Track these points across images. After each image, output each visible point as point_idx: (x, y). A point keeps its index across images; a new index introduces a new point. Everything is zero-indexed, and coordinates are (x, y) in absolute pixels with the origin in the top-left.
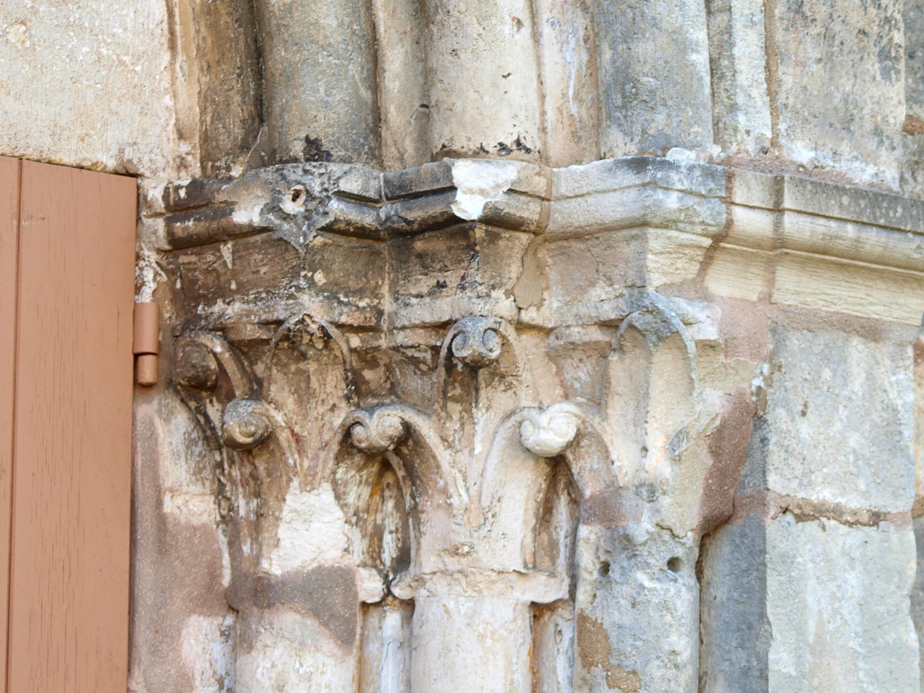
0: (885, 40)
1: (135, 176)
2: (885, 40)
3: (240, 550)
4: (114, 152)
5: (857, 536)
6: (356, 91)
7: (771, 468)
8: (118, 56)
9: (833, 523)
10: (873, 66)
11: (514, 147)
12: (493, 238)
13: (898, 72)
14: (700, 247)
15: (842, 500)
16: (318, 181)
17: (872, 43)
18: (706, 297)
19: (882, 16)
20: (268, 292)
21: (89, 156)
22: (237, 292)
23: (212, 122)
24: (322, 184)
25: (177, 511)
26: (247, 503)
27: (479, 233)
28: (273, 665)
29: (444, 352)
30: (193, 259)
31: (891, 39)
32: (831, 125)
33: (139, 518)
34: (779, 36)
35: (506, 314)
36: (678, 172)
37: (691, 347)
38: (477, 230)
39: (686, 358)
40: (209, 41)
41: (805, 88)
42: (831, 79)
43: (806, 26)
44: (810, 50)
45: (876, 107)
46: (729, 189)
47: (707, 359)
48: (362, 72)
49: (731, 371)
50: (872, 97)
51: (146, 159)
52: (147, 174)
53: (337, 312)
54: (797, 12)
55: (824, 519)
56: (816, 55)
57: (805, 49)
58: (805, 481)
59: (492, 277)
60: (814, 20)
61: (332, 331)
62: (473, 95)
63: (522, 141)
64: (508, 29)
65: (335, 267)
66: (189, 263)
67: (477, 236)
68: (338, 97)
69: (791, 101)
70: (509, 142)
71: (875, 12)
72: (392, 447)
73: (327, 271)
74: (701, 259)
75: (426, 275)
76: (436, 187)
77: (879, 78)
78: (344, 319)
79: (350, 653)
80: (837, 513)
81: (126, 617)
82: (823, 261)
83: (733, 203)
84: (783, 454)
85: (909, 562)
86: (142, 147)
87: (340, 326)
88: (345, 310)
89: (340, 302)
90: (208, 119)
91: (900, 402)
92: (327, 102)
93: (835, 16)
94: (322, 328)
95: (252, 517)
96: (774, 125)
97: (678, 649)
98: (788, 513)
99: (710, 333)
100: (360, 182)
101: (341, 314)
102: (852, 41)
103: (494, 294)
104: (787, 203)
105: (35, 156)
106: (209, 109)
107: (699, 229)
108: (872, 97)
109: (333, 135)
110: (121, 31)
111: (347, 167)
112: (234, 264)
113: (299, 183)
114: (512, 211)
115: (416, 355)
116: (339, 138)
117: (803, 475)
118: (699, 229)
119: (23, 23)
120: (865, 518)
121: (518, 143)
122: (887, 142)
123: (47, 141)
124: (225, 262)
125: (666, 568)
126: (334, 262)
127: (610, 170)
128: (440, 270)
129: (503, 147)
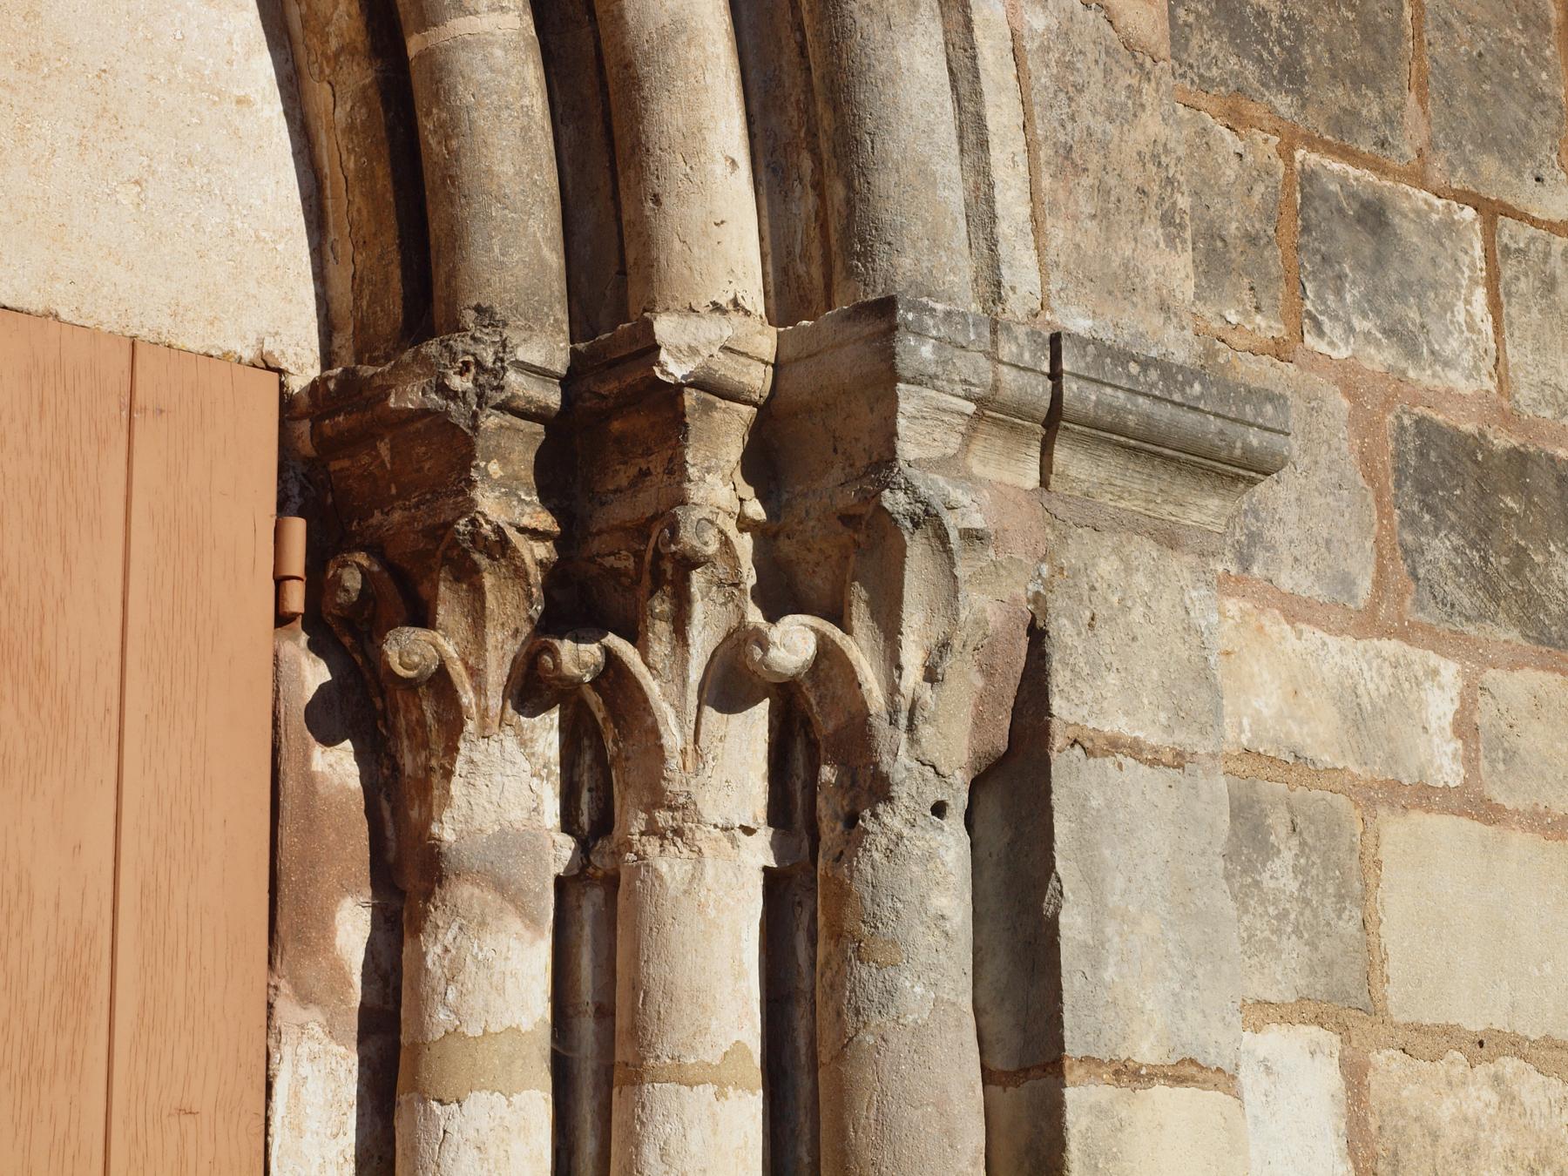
0: (1167, 205)
1: (280, 372)
2: (1167, 205)
3: (407, 816)
4: (252, 341)
5: (1160, 776)
6: (539, 250)
7: (1055, 689)
8: (256, 231)
9: (1131, 761)
10: (1153, 231)
11: (731, 307)
12: (708, 408)
13: (1184, 241)
14: (962, 414)
15: (1141, 735)
16: (491, 351)
17: (1152, 205)
18: (969, 480)
19: (1163, 175)
20: (433, 493)
21: (217, 345)
22: (398, 496)
23: (369, 306)
24: (496, 353)
25: (327, 770)
26: (414, 759)
27: (690, 398)
28: (446, 950)
29: (648, 557)
30: (346, 463)
31: (1174, 203)
32: (1110, 293)
33: (282, 776)
34: (1046, 182)
35: (724, 504)
36: (933, 317)
37: (954, 535)
38: (686, 397)
39: (948, 552)
40: (365, 213)
41: (1078, 246)
42: (1108, 240)
43: (1076, 175)
44: (1082, 203)
45: (1161, 279)
46: (994, 343)
47: (973, 554)
48: (545, 230)
49: (1002, 572)
50: (1156, 267)
51: (290, 352)
52: (292, 369)
53: (517, 511)
54: (1066, 158)
55: (1120, 757)
56: (1088, 209)
57: (1077, 203)
58: (1096, 708)
59: (707, 458)
60: (1085, 170)
61: (512, 534)
62: (677, 245)
63: (740, 301)
64: (720, 168)
65: (514, 456)
66: (342, 469)
67: (687, 403)
68: (516, 257)
69: (1062, 259)
70: (724, 301)
71: (1155, 169)
72: (587, 678)
73: (504, 461)
74: (962, 429)
75: (625, 463)
76: (635, 348)
77: (1162, 245)
78: (525, 521)
79: (542, 935)
80: (1135, 749)
81: (266, 897)
82: (1109, 441)
83: (1001, 362)
84: (1068, 674)
85: (1221, 813)
86: (285, 339)
87: (522, 530)
88: (528, 510)
89: (521, 501)
90: (365, 303)
91: (1203, 623)
92: (502, 263)
93: (1109, 169)
94: (498, 530)
95: (421, 774)
96: (1045, 283)
97: (947, 912)
98: (1077, 747)
99: (977, 521)
100: (543, 352)
101: (522, 515)
102: (1130, 198)
103: (708, 478)
104: (1066, 366)
105: (152, 338)
106: (366, 292)
107: (959, 389)
108: (1156, 267)
109: (511, 301)
110: (259, 202)
111: (525, 335)
112: (393, 463)
113: (466, 353)
114: (729, 374)
115: (618, 564)
116: (517, 305)
117: (1096, 701)
118: (959, 389)
119: (137, 183)
120: (1167, 757)
121: (735, 302)
122: (1175, 320)
123: (165, 323)
124: (383, 462)
125: (929, 813)
126: (512, 451)
127: (849, 318)
128: (642, 456)
129: (716, 307)
